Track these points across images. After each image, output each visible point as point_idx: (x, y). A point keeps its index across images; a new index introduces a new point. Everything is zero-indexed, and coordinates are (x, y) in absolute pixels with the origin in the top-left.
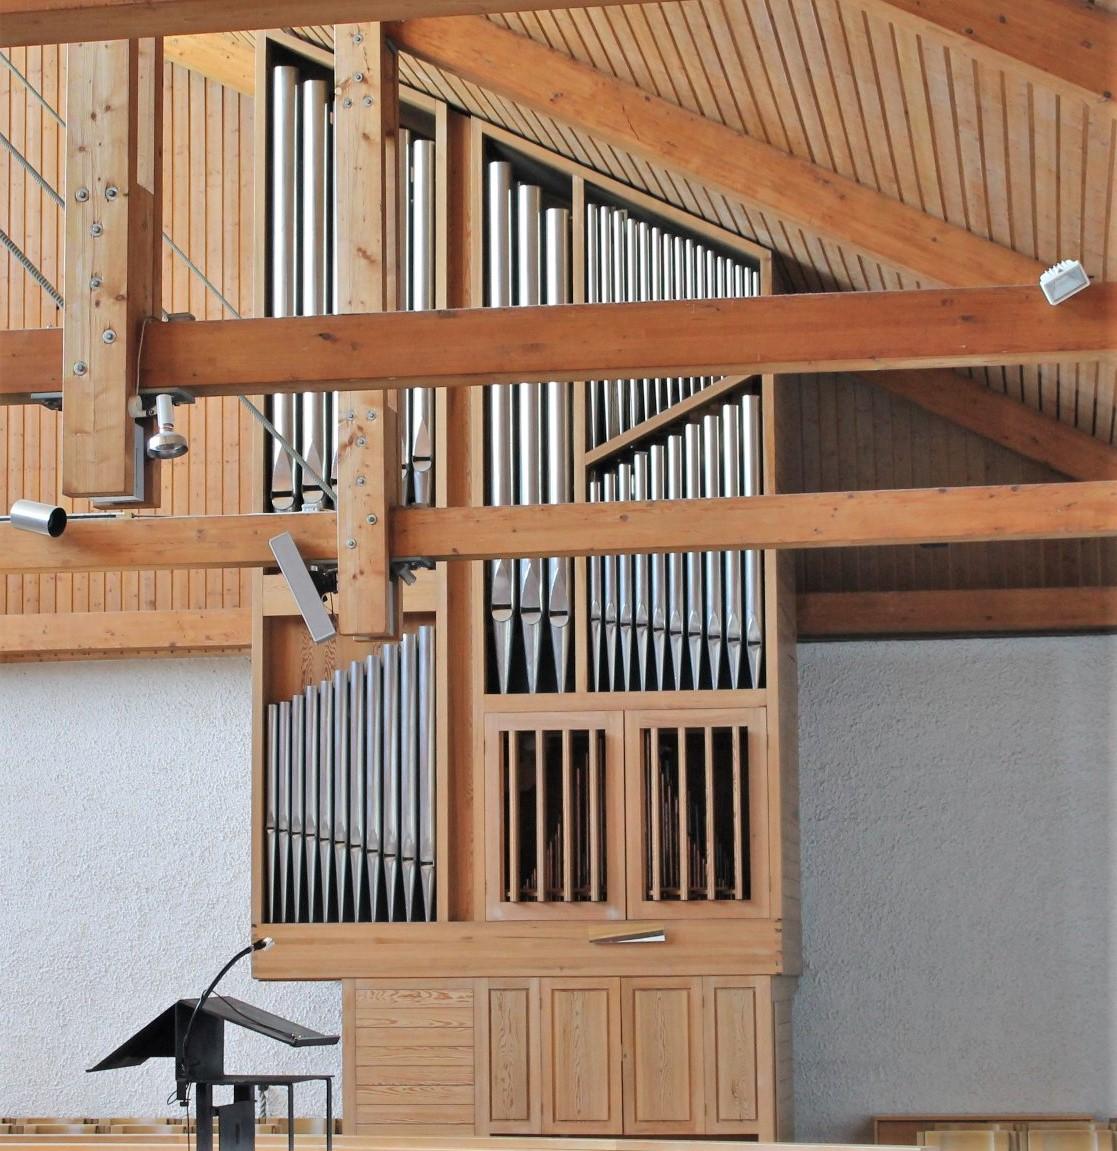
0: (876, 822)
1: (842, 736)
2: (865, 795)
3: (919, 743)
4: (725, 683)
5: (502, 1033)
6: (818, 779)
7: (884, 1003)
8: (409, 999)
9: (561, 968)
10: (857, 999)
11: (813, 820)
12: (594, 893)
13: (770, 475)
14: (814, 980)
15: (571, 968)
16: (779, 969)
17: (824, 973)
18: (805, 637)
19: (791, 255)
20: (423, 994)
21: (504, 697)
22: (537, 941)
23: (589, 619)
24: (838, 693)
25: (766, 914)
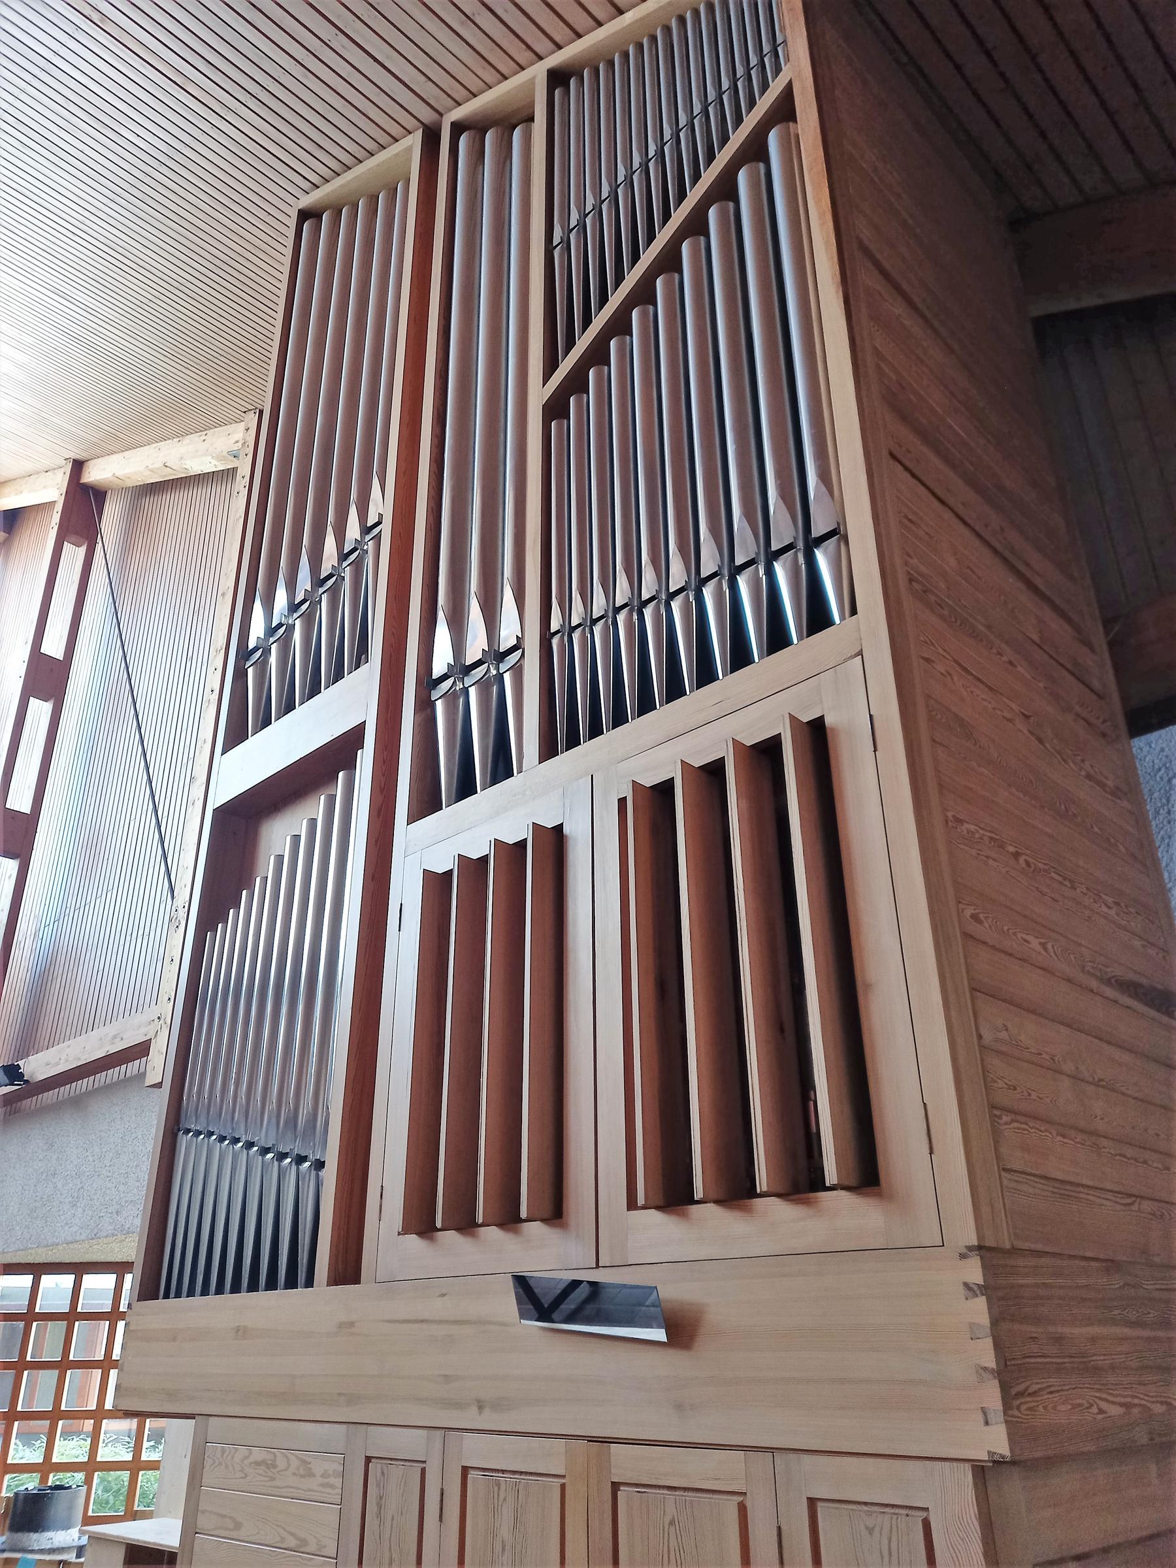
20: (281, 1463)
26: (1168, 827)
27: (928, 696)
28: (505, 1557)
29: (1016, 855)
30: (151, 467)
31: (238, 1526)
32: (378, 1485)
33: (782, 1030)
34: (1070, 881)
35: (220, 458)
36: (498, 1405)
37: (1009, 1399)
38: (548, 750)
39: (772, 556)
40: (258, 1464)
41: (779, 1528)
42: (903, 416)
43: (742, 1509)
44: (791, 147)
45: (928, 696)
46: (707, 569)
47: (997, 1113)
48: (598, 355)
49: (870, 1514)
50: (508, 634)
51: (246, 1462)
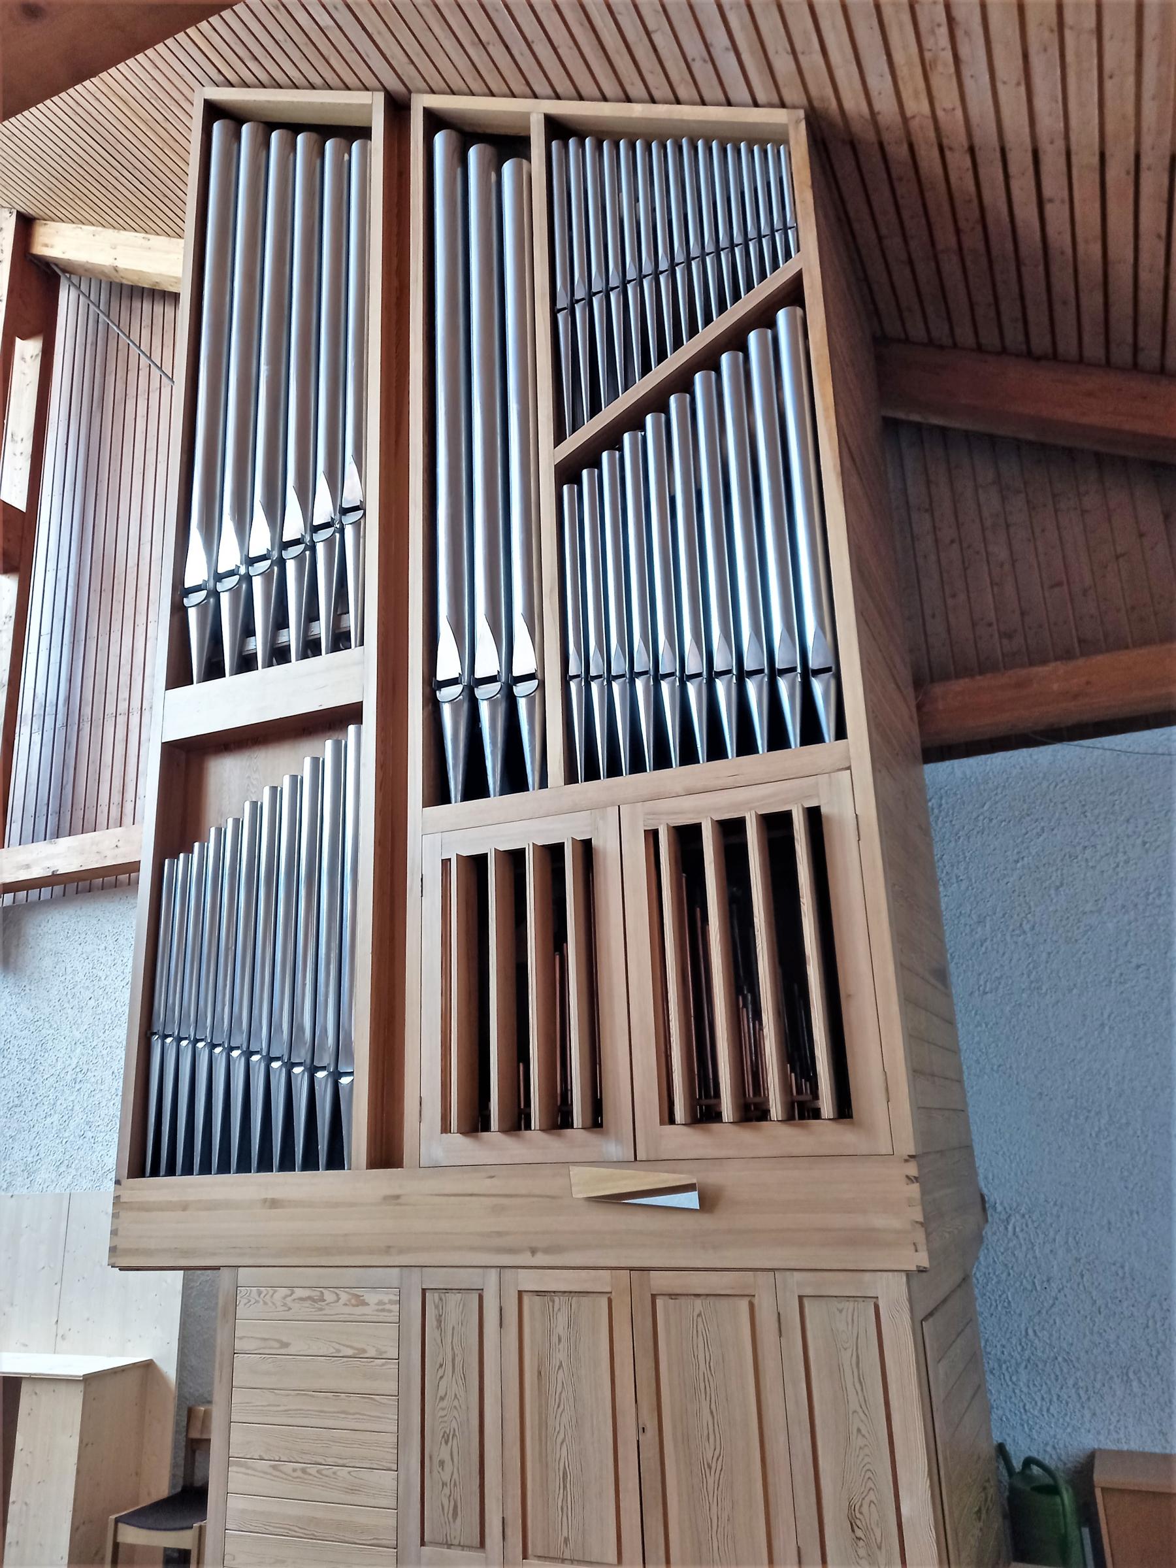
0: (1070, 990)
1: (1005, 876)
2: (1049, 954)
3: (1122, 875)
4: (778, 740)
5: (440, 1373)
7: (1122, 1267)
8: (307, 1304)
9: (534, 1251)
10: (1078, 1260)
11: (976, 994)
12: (826, 1103)
13: (826, 409)
14: (1006, 1228)
15: (547, 1250)
17: (1018, 1217)
18: (937, 752)
19: (838, 119)
20: (329, 1296)
21: (458, 810)
22: (495, 1200)
23: (566, 679)
24: (991, 820)
25: (884, 1147)
28: (561, 1346)
32: (437, 1307)
38: (571, 777)
40: (301, 1299)
44: (803, 329)
48: (610, 439)
50: (524, 663)
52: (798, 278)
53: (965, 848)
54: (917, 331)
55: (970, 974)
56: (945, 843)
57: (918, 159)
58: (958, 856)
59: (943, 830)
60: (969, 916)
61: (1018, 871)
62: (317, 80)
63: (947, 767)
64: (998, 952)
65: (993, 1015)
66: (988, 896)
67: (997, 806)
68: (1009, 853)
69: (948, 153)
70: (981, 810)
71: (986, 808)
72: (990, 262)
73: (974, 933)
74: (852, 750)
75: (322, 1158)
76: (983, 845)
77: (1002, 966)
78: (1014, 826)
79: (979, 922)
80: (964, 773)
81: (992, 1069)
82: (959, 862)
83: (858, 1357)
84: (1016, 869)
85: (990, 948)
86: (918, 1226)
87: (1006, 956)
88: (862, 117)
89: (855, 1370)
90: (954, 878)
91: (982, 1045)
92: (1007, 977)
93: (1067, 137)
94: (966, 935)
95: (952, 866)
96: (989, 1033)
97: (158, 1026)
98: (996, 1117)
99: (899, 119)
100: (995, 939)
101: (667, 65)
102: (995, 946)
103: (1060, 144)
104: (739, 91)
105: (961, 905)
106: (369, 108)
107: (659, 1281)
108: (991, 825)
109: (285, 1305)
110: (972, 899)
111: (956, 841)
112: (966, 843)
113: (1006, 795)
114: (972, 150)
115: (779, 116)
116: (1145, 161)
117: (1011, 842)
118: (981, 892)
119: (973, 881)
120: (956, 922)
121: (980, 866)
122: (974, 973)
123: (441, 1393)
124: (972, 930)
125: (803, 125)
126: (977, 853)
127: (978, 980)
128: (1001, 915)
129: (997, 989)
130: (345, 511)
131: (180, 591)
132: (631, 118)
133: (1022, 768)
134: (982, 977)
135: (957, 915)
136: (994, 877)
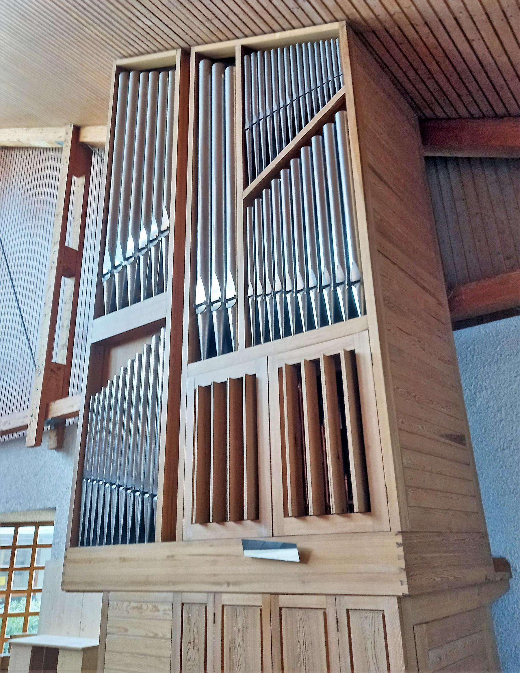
1: (510, 385)
6: (498, 419)
11: (499, 450)
13: (356, 156)
16: (404, 590)
20: (144, 606)
24: (501, 355)
26: (466, 366)
27: (389, 344)
28: (240, 634)
29: (415, 396)
30: (11, 140)
31: (126, 630)
32: (188, 612)
33: (339, 458)
34: (432, 401)
35: (49, 143)
36: (236, 583)
37: (409, 577)
38: (248, 344)
39: (336, 285)
40: (134, 608)
41: (337, 619)
42: (382, 233)
43: (325, 614)
44: (344, 121)
45: (389, 344)
46: (311, 285)
47: (407, 488)
48: (266, 184)
49: (366, 613)
50: (230, 293)
51: (129, 608)
52: (344, 97)
53: (489, 371)
54: (463, 112)
55: (495, 439)
56: (479, 369)
57: (405, 32)
58: (485, 375)
59: (477, 362)
60: (493, 407)
61: (517, 382)
62: (155, 49)
63: (477, 329)
64: (509, 427)
65: (509, 462)
66: (502, 396)
67: (504, 347)
68: (512, 372)
69: (416, 27)
70: (496, 350)
71: (498, 349)
72: (458, 74)
73: (496, 417)
74: (369, 322)
75: (146, 537)
76: (498, 369)
77: (512, 434)
78: (513, 358)
79: (498, 411)
80: (486, 331)
81: (510, 491)
82: (486, 379)
83: (374, 643)
84: (516, 381)
85: (505, 424)
86: (402, 571)
87: (514, 428)
88: (372, 19)
89: (373, 651)
90: (484, 387)
91: (504, 478)
92: (515, 441)
93: (466, 9)
94: (492, 418)
95: (483, 381)
96: (507, 471)
97: (86, 475)
98: (514, 519)
99: (388, 16)
100: (507, 420)
101: (283, 13)
102: (508, 423)
103: (465, 13)
104: (316, 19)
105: (488, 402)
106: (174, 57)
107: (283, 601)
108: (501, 358)
109: (127, 610)
110: (494, 398)
111: (484, 368)
112: (489, 368)
113: (508, 342)
114: (426, 23)
115: (335, 26)
116: (508, 14)
117: (512, 366)
118: (498, 394)
119: (494, 388)
120: (486, 411)
121: (497, 380)
122: (498, 438)
123: (189, 657)
124: (495, 415)
125: (345, 27)
126: (495, 373)
127: (500, 442)
128: (510, 406)
129: (510, 446)
130: (162, 232)
131: (101, 275)
132: (275, 40)
133: (515, 327)
134: (502, 441)
135: (487, 407)
136: (505, 385)
